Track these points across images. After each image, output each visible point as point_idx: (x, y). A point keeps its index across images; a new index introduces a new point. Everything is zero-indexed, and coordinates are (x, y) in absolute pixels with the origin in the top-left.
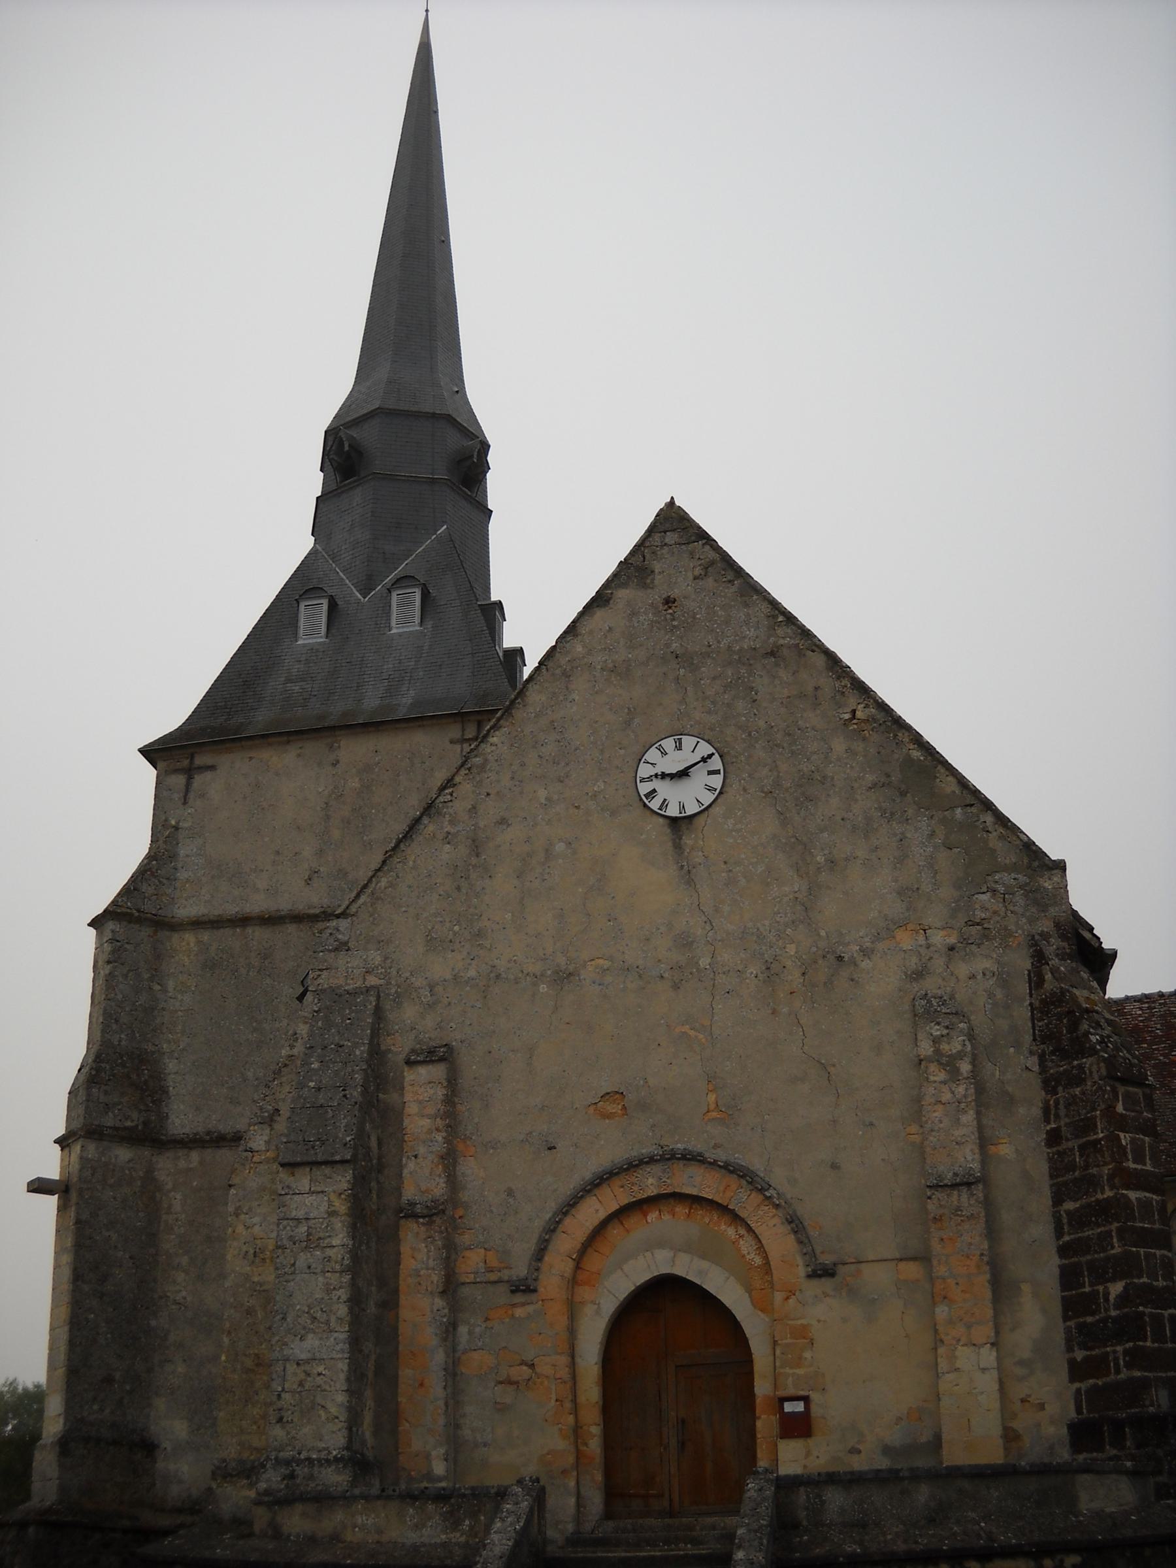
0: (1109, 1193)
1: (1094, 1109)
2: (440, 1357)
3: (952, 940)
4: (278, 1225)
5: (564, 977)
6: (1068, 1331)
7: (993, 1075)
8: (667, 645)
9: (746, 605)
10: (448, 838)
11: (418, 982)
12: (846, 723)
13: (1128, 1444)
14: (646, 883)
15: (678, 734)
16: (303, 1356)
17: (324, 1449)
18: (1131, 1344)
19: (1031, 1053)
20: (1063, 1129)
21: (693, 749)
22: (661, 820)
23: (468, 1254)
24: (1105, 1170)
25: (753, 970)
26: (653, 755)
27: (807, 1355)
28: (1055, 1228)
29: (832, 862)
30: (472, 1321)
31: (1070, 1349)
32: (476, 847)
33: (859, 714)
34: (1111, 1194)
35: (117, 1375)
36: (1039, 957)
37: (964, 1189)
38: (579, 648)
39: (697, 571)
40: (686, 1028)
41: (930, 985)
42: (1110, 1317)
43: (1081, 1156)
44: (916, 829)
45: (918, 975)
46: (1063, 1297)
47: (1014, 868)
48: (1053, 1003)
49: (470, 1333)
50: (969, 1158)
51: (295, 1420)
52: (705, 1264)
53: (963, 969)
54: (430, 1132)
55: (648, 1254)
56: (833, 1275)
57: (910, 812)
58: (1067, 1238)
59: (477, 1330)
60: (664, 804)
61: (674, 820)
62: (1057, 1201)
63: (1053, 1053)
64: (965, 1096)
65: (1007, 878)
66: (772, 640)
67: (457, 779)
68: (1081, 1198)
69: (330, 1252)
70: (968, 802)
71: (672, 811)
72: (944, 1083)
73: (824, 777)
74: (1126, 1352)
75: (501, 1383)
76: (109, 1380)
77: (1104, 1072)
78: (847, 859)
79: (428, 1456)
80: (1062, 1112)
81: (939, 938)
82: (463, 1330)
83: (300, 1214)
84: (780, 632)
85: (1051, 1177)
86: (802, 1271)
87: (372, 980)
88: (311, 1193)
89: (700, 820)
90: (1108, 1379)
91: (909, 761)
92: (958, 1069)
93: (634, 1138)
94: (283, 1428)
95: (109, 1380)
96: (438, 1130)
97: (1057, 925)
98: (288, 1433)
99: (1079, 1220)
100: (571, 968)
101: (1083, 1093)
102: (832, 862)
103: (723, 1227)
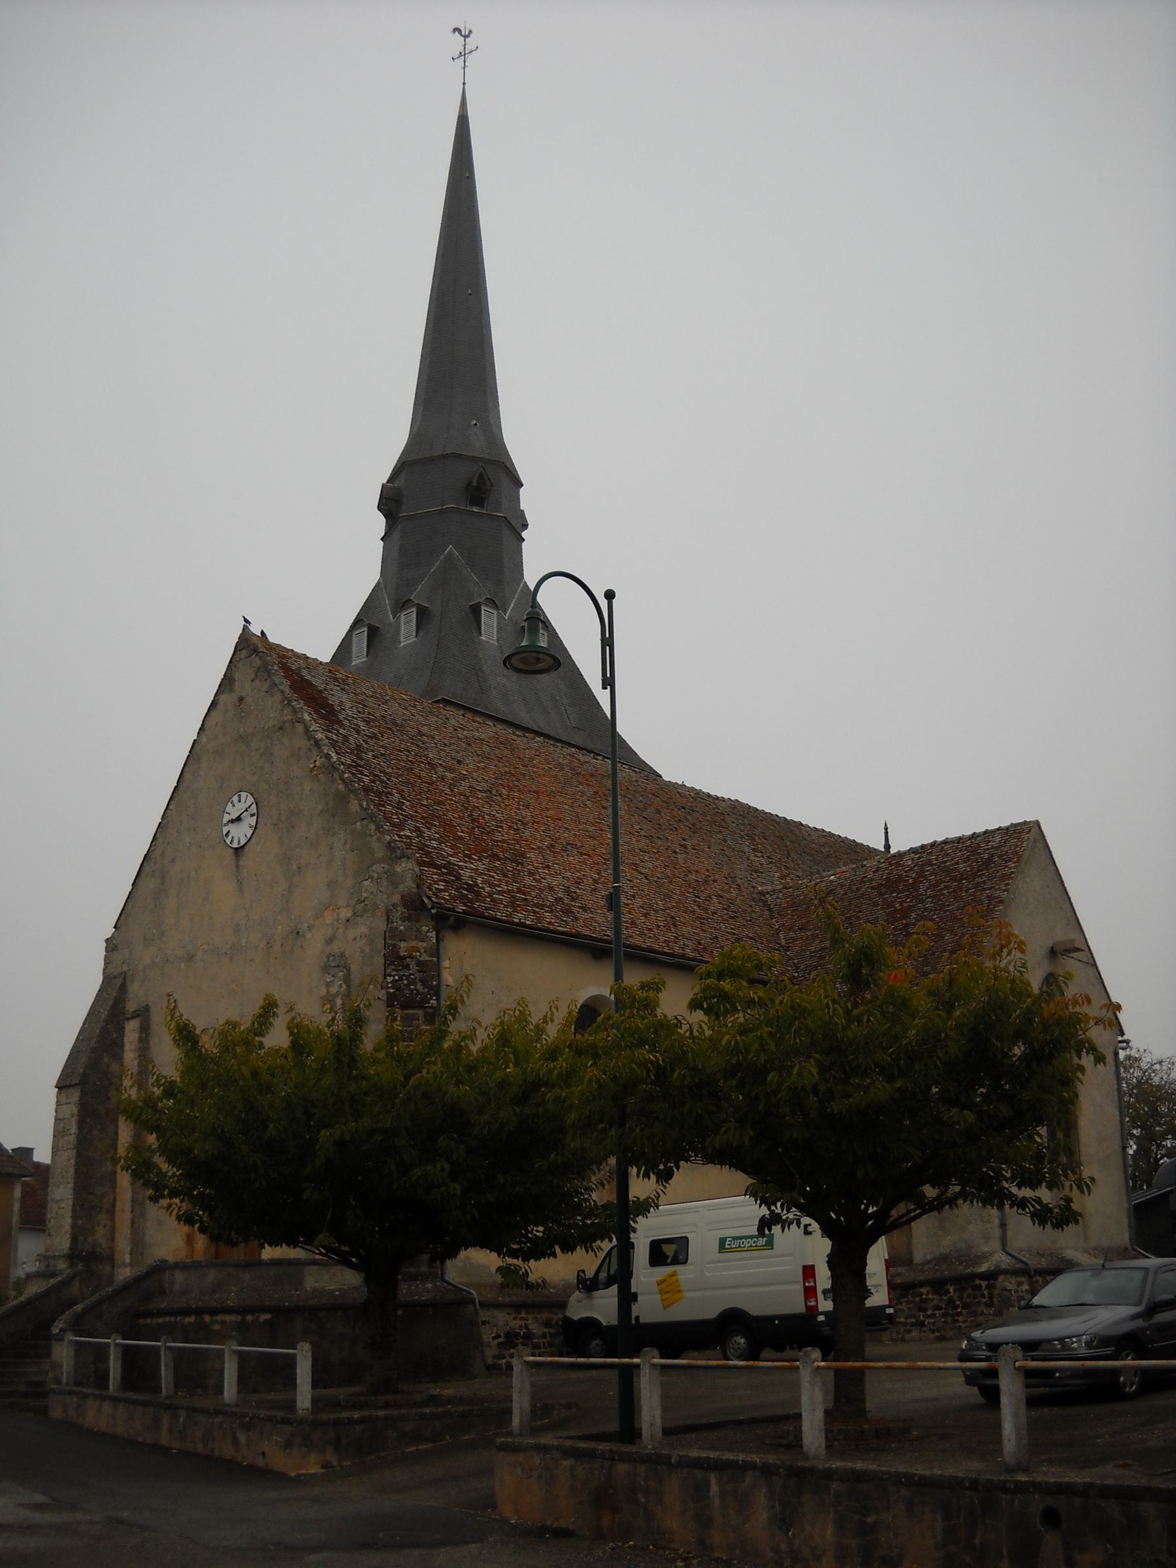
3: (349, 915)
25: (262, 945)
26: (229, 808)
53: (352, 934)
61: (236, 849)
71: (235, 845)
89: (247, 848)
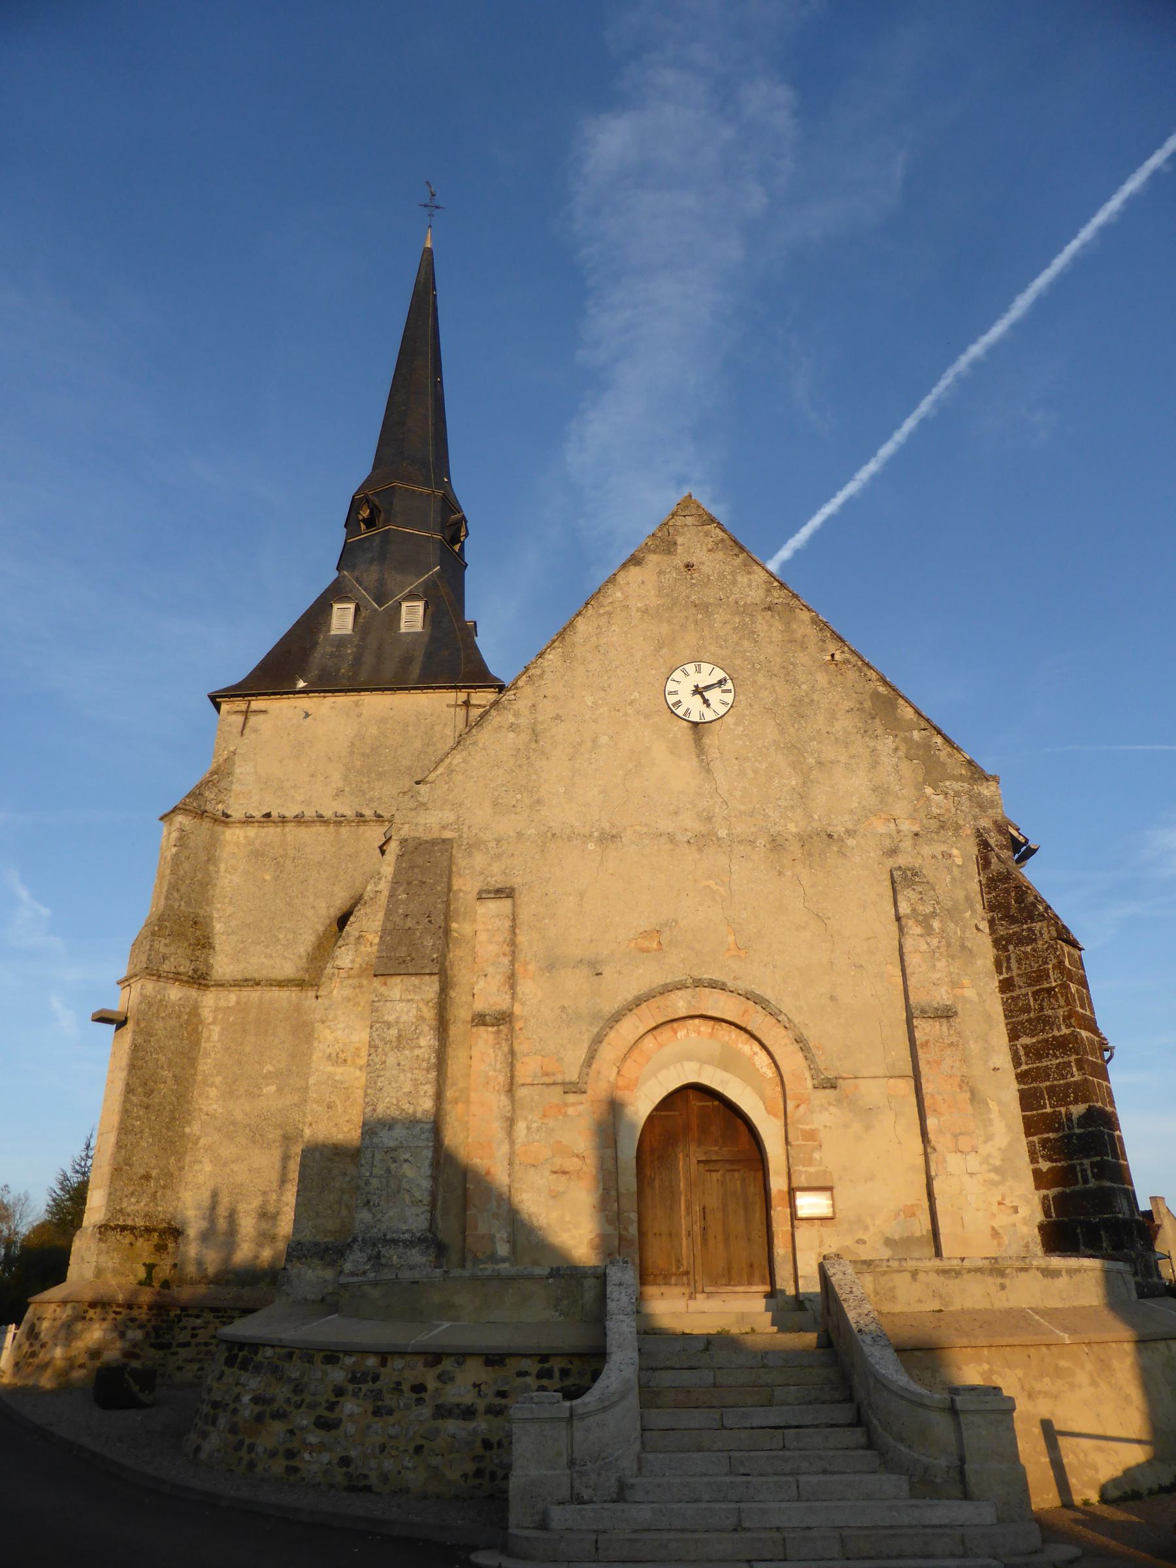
0: (1065, 1031)
1: (1045, 963)
2: (505, 1148)
3: (916, 828)
4: (371, 1027)
5: (609, 838)
6: (1031, 1145)
7: (956, 933)
8: (688, 597)
9: (749, 573)
10: (512, 727)
11: (486, 836)
12: (826, 664)
13: (1105, 1245)
14: (676, 771)
15: (697, 661)
16: (391, 1144)
17: (408, 1231)
18: (1099, 1158)
19: (983, 919)
20: (1016, 979)
21: (709, 674)
22: (685, 723)
23: (526, 1059)
24: (1061, 1012)
27: (817, 1155)
28: (1013, 1059)
29: (820, 763)
30: (530, 1117)
31: (1033, 1160)
32: (535, 736)
33: (838, 657)
34: (1068, 1032)
35: (154, 1173)
36: (984, 845)
37: (944, 1021)
38: (619, 594)
39: (710, 547)
40: (711, 883)
41: (902, 860)
42: (1075, 1134)
43: (1035, 1000)
44: (884, 744)
45: (893, 852)
46: (1024, 1117)
47: (961, 778)
48: (1000, 881)
49: (528, 1128)
50: (945, 997)
51: (382, 1203)
52: (726, 1076)
53: (927, 850)
54: (497, 956)
55: (678, 1065)
56: (834, 1087)
57: (879, 732)
58: (1024, 1067)
59: (535, 1125)
60: (688, 712)
61: (696, 724)
62: (1013, 1036)
63: (1001, 919)
64: (938, 947)
65: (957, 786)
66: (769, 599)
67: (520, 683)
68: (1037, 1034)
69: (417, 1052)
70: (922, 726)
72: (921, 935)
73: (812, 701)
74: (1093, 1165)
75: (555, 1172)
76: (147, 1177)
77: (1054, 934)
78: (831, 762)
79: (492, 1238)
80: (1014, 965)
81: (907, 826)
82: (521, 1126)
83: (391, 1018)
84: (775, 594)
85: (1006, 1017)
86: (809, 1084)
87: (448, 834)
88: (401, 1000)
90: (1077, 1188)
91: (876, 695)
92: (931, 926)
93: (674, 968)
94: (370, 1210)
95: (147, 1177)
96: (504, 954)
97: (995, 822)
98: (374, 1216)
99: (1035, 1052)
100: (614, 832)
101: (1034, 950)
102: (820, 763)
103: (740, 1045)
